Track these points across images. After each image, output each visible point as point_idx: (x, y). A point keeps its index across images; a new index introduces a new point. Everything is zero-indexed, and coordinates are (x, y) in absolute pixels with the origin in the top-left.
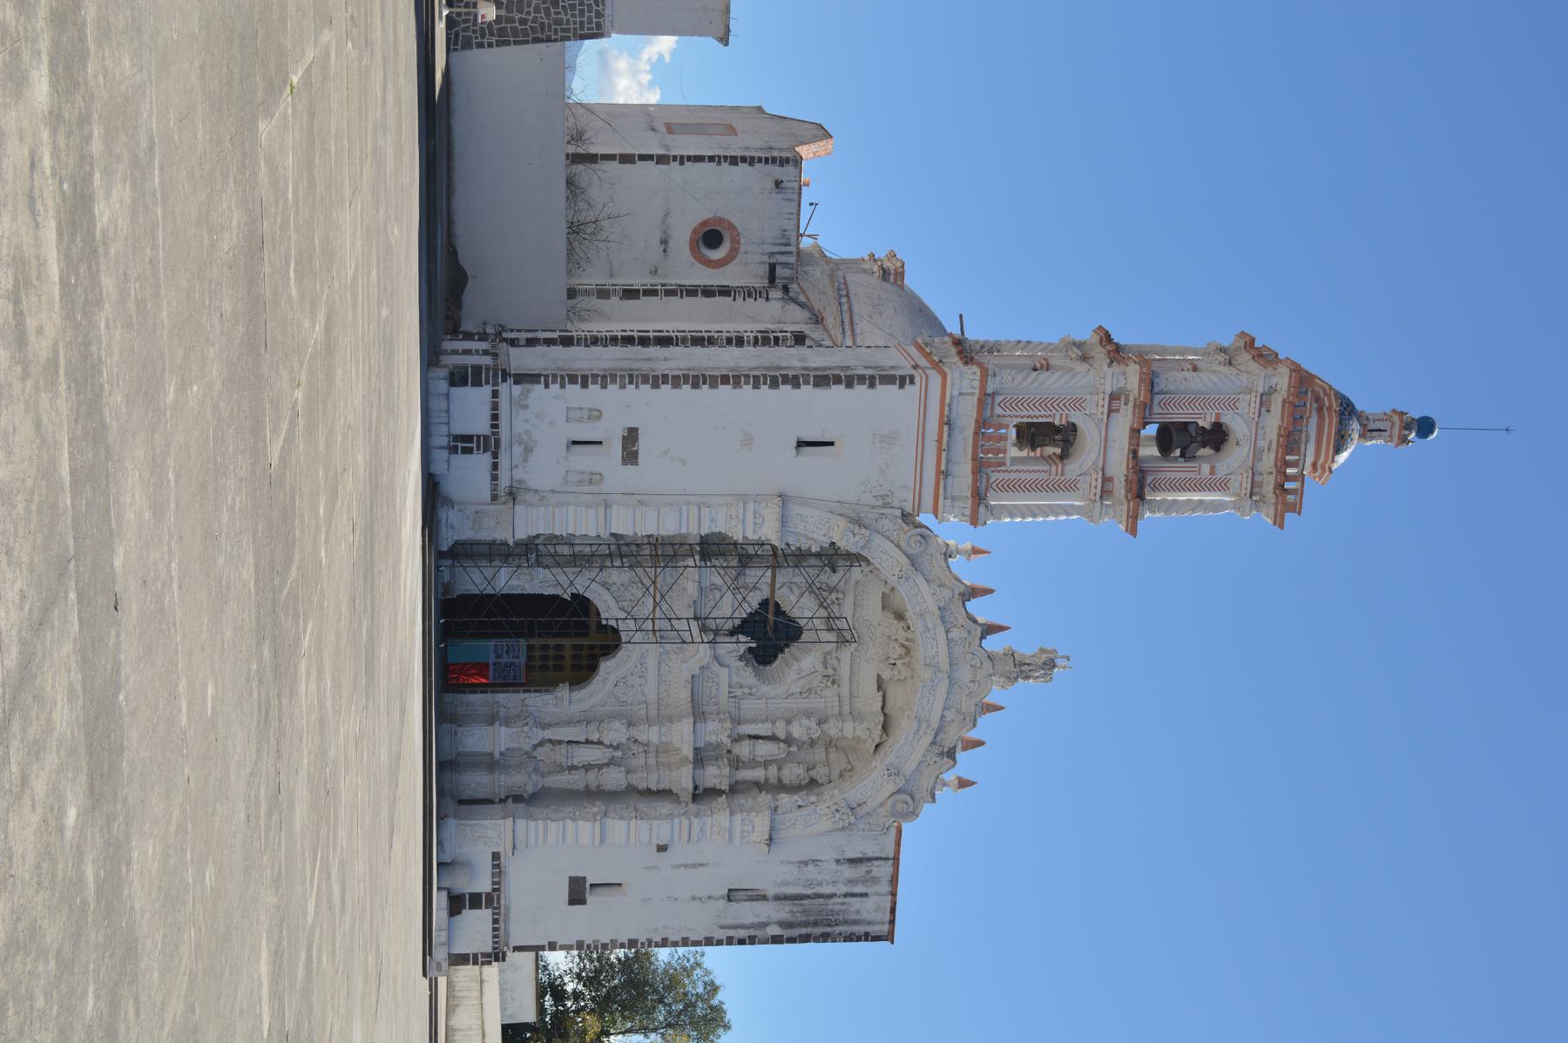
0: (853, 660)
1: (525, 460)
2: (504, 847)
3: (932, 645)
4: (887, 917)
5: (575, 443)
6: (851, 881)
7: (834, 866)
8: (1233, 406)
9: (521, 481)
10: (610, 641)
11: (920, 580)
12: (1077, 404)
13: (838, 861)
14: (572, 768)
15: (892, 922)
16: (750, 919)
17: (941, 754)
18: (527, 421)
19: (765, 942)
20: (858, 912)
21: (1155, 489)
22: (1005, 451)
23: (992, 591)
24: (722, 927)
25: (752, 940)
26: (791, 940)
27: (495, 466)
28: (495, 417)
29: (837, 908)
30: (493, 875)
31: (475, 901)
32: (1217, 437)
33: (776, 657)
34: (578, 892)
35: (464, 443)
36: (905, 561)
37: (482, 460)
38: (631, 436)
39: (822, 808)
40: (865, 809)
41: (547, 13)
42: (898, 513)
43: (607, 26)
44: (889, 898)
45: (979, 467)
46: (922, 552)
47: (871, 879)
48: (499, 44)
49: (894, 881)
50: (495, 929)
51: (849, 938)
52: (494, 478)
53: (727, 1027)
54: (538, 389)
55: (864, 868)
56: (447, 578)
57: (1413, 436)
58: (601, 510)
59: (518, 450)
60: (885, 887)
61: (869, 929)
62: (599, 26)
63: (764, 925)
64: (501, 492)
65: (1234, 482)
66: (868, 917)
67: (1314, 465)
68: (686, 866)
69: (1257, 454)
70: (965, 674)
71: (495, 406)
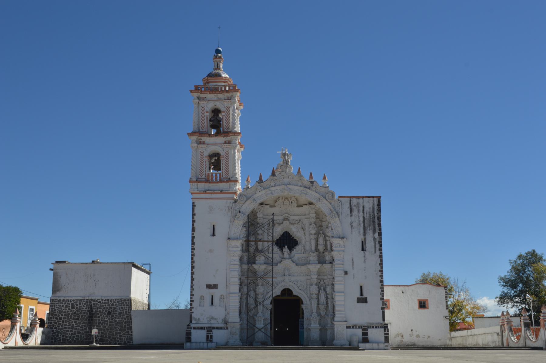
0: (294, 215)
1: (216, 319)
2: (344, 325)
3: (277, 191)
4: (372, 199)
5: (212, 303)
6: (358, 211)
7: (353, 217)
8: (203, 108)
9: (223, 320)
10: (287, 292)
11: (255, 196)
13: (351, 216)
14: (327, 303)
15: (373, 197)
18: (203, 319)
19: (381, 238)
20: (370, 208)
21: (229, 128)
22: (212, 174)
23: (311, 174)
24: (375, 252)
26: (380, 230)
27: (217, 328)
28: (202, 328)
29: (368, 215)
30: (356, 328)
31: (365, 334)
32: (216, 112)
33: (295, 239)
34: (362, 300)
35: (209, 338)
37: (215, 332)
38: (209, 287)
40: (332, 208)
41: (124, 315)
42: (234, 204)
43: (128, 298)
44: (364, 199)
46: (245, 196)
47: (358, 205)
48: (131, 329)
49: (358, 198)
50: (376, 327)
51: (379, 210)
52: (221, 328)
53: (534, 251)
54: (193, 315)
55: (354, 208)
56: (260, 344)
57: (220, 55)
58: (231, 295)
59: (212, 321)
60: (361, 200)
61: (376, 204)
62: (128, 300)
63: (375, 239)
64: (225, 326)
65: (227, 105)
66: (371, 206)
67: (225, 82)
68: (353, 265)
69: (219, 99)
70: (286, 180)
71: (198, 328)
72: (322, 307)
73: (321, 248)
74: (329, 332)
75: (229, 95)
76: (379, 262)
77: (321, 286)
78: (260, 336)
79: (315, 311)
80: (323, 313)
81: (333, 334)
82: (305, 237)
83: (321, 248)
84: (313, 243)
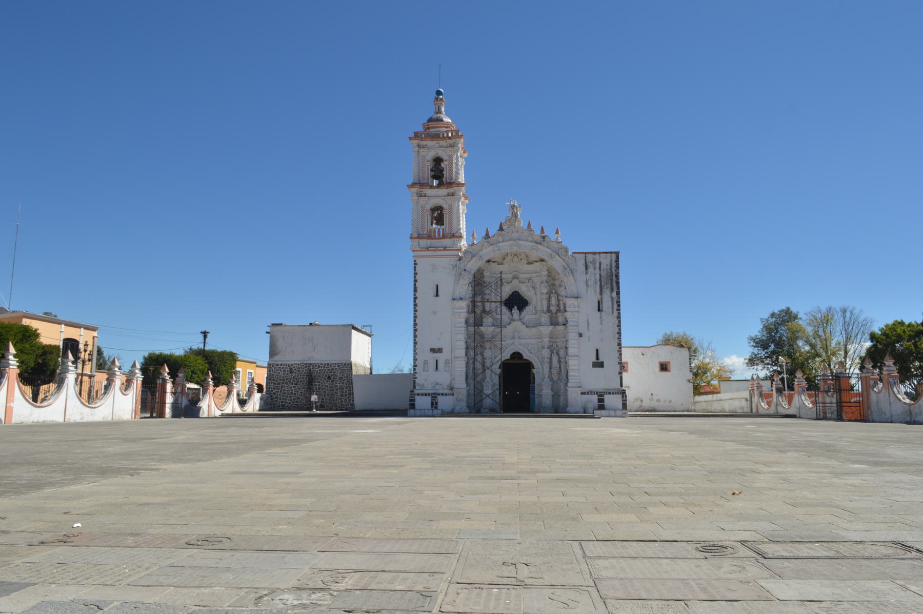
2: (579, 391)
3: (505, 247)
10: (517, 355)
11: (482, 253)
12: (423, 207)
16: (610, 304)
25: (618, 302)
26: (618, 288)
31: (601, 400)
32: (438, 161)
34: (599, 364)
35: (434, 405)
37: (440, 398)
38: (433, 350)
39: (565, 280)
45: (444, 237)
46: (471, 253)
47: (594, 262)
49: (594, 253)
51: (617, 267)
53: (788, 308)
60: (597, 256)
63: (612, 298)
64: (450, 392)
65: (449, 153)
69: (441, 147)
70: (515, 235)
71: (422, 394)
72: (554, 372)
74: (562, 398)
75: (451, 142)
76: (417, 301)
77: (553, 350)
78: (488, 402)
79: (546, 376)
80: (555, 378)
81: (567, 401)
82: (536, 296)
84: (545, 303)
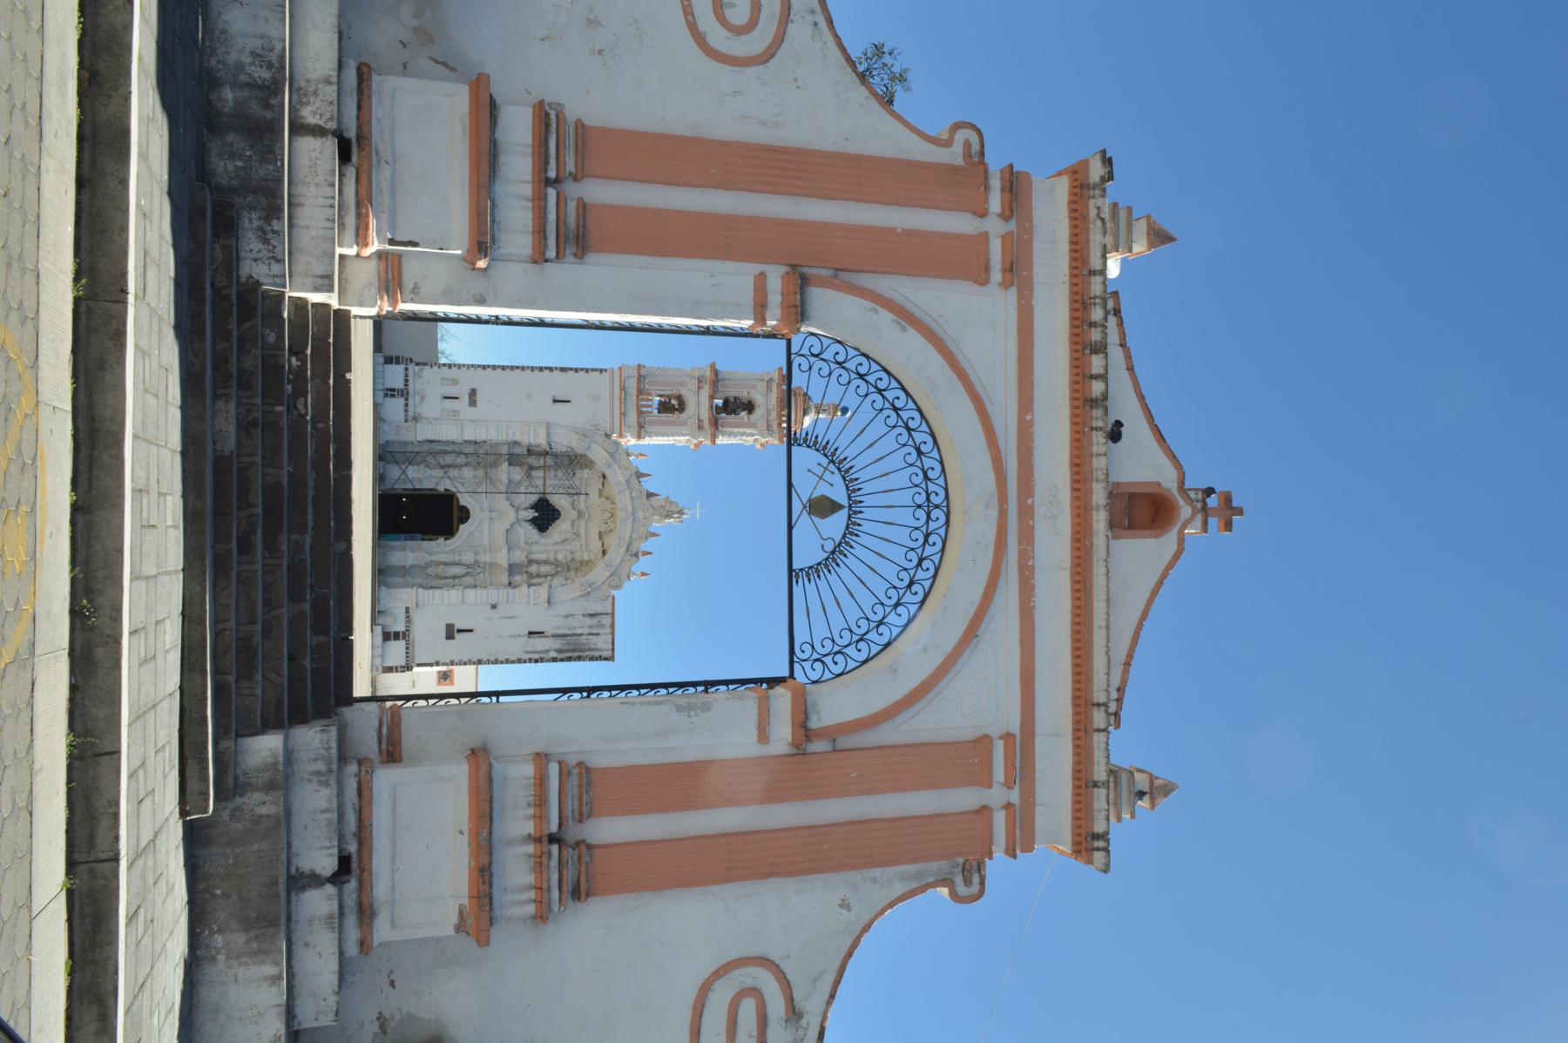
2: (411, 604)
3: (624, 501)
10: (465, 515)
16: (540, 648)
17: (592, 52)
25: (542, 660)
31: (397, 636)
32: (749, 407)
34: (451, 632)
35: (391, 393)
36: (607, 456)
37: (400, 401)
38: (473, 393)
39: (575, 585)
45: (640, 413)
46: (616, 451)
51: (592, 659)
54: (427, 368)
69: (768, 412)
70: (640, 515)
73: (534, 569)
74: (400, 580)
79: (434, 558)
80: (430, 570)
83: (534, 569)
84: (543, 557)
